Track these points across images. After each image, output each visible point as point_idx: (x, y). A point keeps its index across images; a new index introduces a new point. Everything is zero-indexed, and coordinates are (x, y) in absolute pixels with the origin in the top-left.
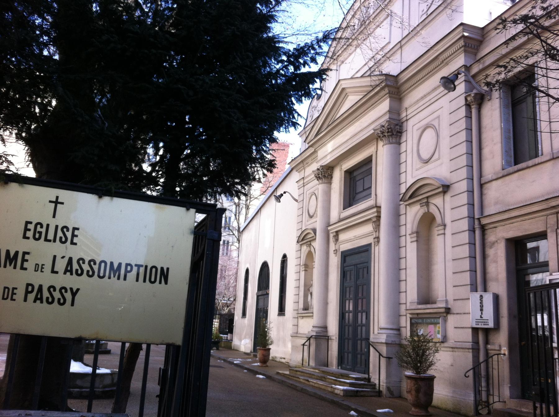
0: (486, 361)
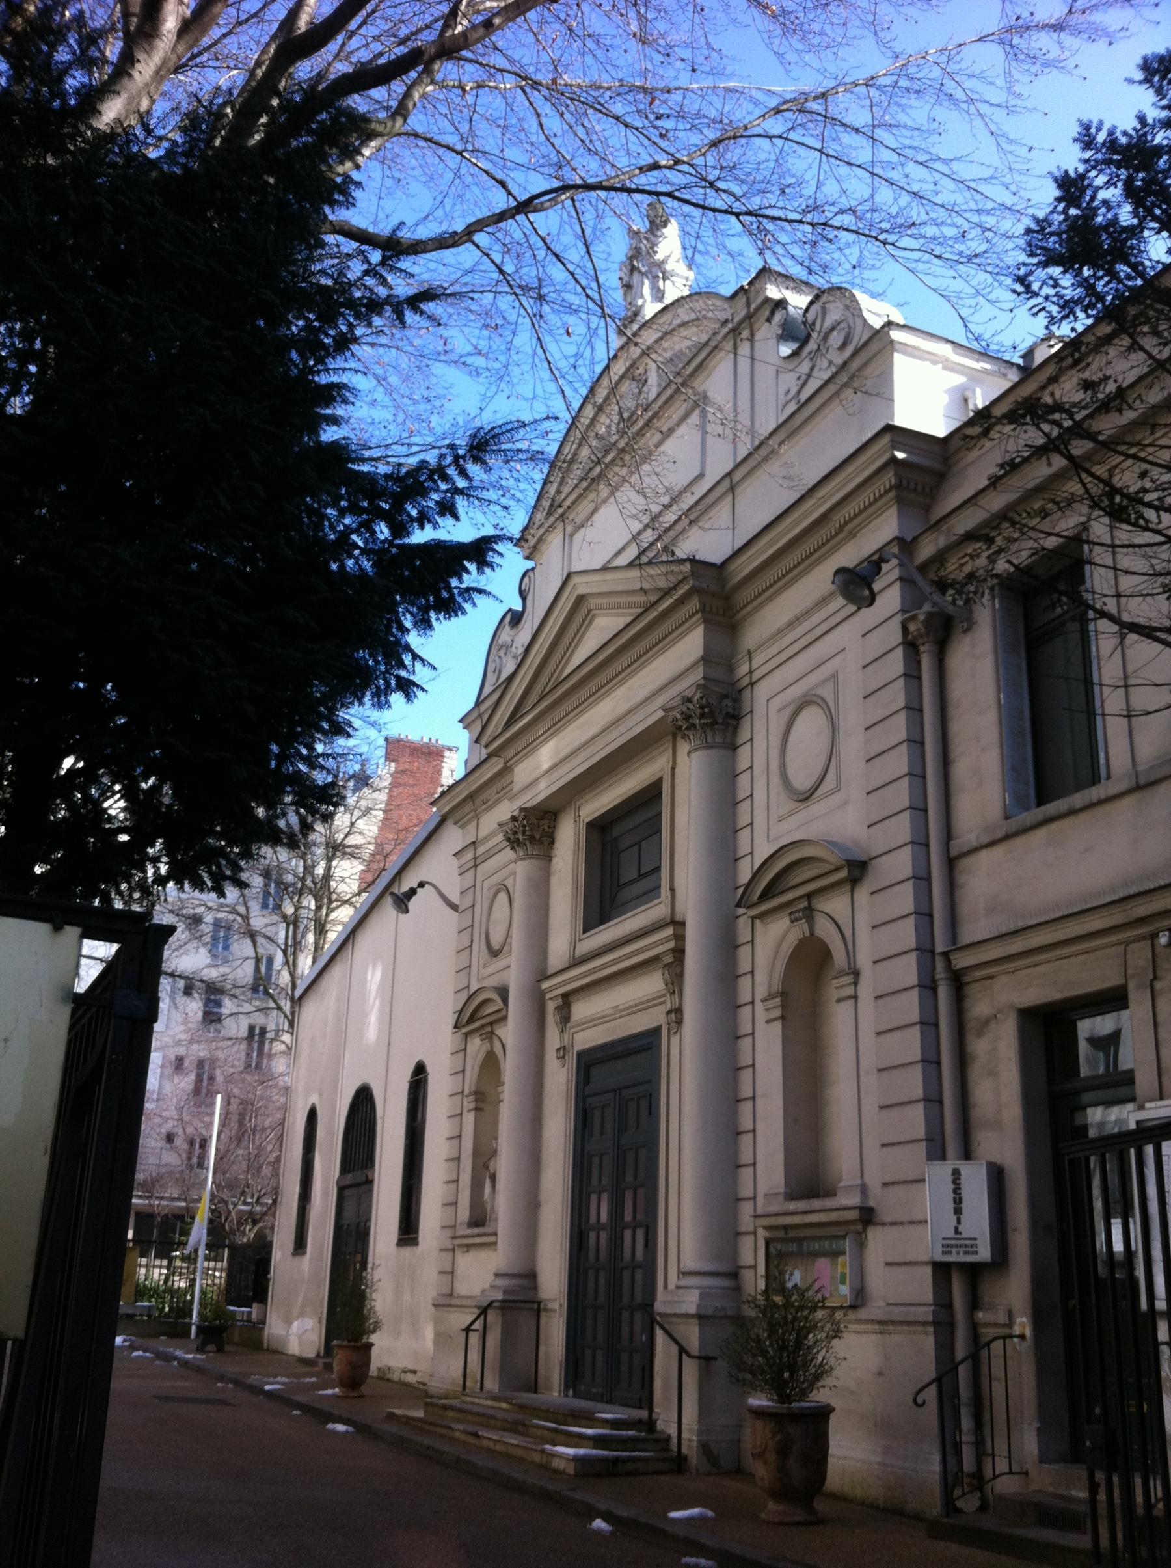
0: (974, 1358)
